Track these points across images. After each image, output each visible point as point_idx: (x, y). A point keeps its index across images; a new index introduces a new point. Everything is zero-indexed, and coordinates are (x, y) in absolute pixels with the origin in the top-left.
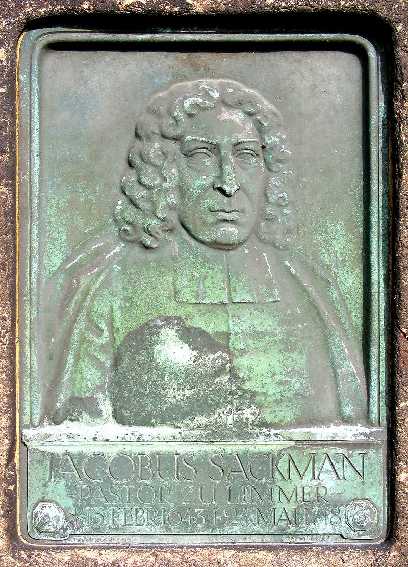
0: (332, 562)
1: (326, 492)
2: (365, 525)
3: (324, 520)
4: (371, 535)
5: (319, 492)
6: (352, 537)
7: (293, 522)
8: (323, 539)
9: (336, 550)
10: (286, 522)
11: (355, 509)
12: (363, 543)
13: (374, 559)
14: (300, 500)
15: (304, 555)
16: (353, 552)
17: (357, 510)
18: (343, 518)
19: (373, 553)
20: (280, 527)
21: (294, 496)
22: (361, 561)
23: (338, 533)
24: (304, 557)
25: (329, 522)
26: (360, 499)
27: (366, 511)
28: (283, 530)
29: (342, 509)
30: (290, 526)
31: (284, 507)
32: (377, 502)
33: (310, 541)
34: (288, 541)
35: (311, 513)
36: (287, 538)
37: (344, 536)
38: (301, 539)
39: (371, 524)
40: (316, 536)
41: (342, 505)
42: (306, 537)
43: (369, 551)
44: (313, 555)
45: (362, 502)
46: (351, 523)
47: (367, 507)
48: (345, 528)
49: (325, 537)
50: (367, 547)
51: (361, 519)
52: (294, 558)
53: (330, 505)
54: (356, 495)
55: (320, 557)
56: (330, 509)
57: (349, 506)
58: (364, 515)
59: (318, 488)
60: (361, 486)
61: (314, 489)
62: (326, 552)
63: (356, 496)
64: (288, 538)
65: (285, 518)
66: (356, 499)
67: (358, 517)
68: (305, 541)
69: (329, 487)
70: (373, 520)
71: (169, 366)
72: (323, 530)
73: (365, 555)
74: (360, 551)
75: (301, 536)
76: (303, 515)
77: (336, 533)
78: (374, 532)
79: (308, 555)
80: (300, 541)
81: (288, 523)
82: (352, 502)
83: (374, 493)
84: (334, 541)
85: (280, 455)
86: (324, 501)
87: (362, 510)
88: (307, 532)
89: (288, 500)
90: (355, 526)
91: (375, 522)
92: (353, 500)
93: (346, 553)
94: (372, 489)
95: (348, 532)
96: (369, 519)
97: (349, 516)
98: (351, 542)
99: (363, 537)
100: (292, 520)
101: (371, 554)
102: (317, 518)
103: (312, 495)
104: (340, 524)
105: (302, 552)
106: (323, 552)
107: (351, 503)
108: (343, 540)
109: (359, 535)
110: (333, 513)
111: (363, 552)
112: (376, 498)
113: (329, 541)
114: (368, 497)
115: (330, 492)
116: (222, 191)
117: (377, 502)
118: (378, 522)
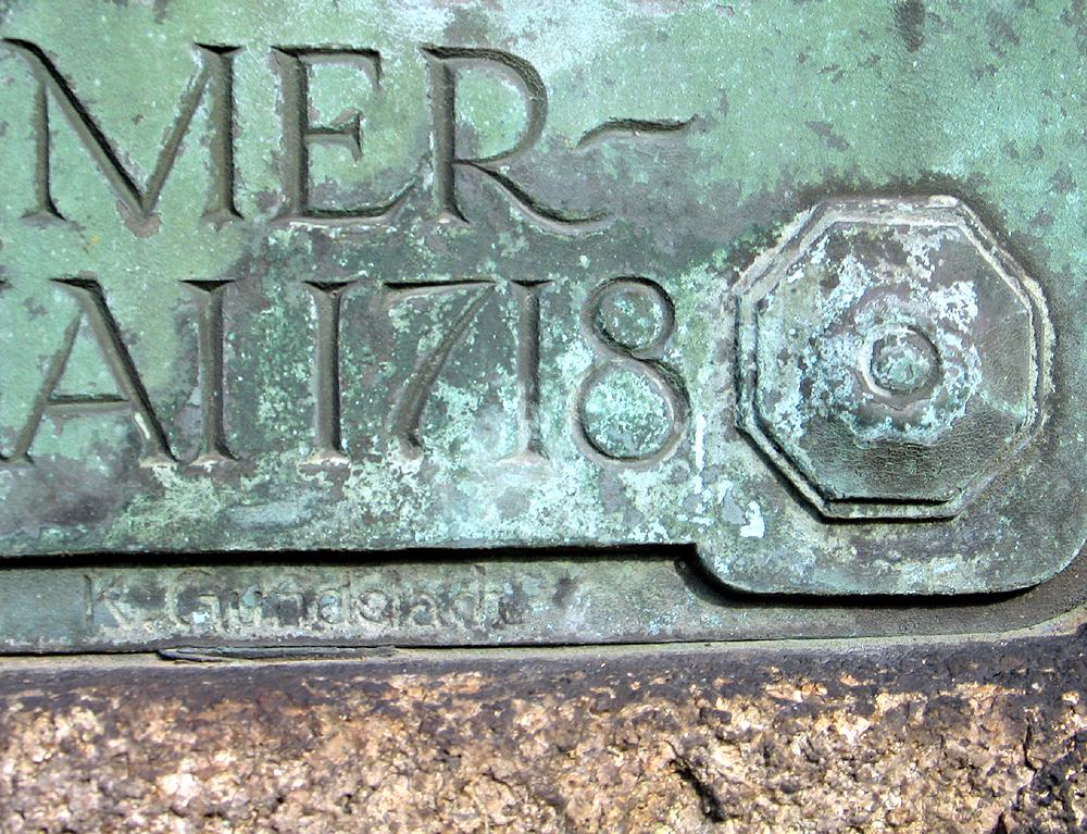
0: (593, 811)
1: (538, 112)
2: (929, 437)
3: (514, 404)
4: (987, 545)
5: (464, 115)
6: (798, 573)
7: (193, 423)
8: (511, 609)
9: (635, 697)
10: (111, 429)
11: (830, 283)
12: (908, 641)
13: (1027, 777)
14: (264, 200)
15: (292, 748)
16: (811, 710)
17: (851, 285)
18: (708, 378)
19: (1011, 711)
20: (48, 475)
21: (196, 157)
22: (893, 800)
23: (655, 533)
24: (291, 775)
25: (570, 428)
26: (887, 191)
27: (939, 298)
28: (88, 511)
29: (701, 288)
30: (164, 470)
31: (90, 268)
32: (1043, 220)
33: (372, 631)
34: (151, 632)
35: (378, 333)
36: (136, 598)
37: (721, 568)
38: (286, 613)
39: (985, 430)
40: (432, 579)
41: (694, 251)
42: (331, 584)
43: (978, 695)
44: (389, 749)
45: (901, 214)
46: (788, 415)
47: (953, 265)
48: (724, 486)
49: (529, 585)
50: (955, 665)
51: (895, 369)
52: (180, 784)
53: (572, 248)
54: (838, 143)
55: (467, 769)
56: (580, 292)
57: (763, 259)
58: (922, 336)
59: (449, 77)
60: (889, 48)
61: (408, 75)
62: (533, 716)
63: (838, 161)
64: (149, 599)
65: (105, 379)
66: (843, 189)
67: (862, 358)
68: (329, 631)
69: (566, 62)
70: (1014, 390)
71: (1063, 727)
72: (512, 505)
73: (931, 733)
74: (885, 702)
75: (285, 583)
76: (290, 351)
77: (638, 537)
78: (1020, 522)
79: (335, 749)
80: (275, 629)
81: (133, 437)
82: (803, 217)
83: (1022, 128)
84: (617, 629)
85: (759, 732)
86: (517, 211)
87: (904, 291)
88: (337, 529)
89: (139, 198)
90: (825, 452)
91: (1024, 410)
92: (810, 197)
93: (742, 721)
94: (1004, 81)
95: (755, 528)
96: (969, 378)
97: (767, 358)
98: (788, 634)
99: (910, 578)
100: (180, 404)
101: (998, 724)
102: (444, 391)
103: (385, 149)
104: (675, 441)
105: (270, 721)
106: (497, 722)
107: (789, 231)
108: (713, 616)
109: (866, 552)
110: (606, 336)
111: (908, 708)
112: (1037, 182)
113: (573, 621)
114: (954, 166)
115: (573, 118)
116: (326, 287)
117: (1043, 220)
118: (1057, 415)
